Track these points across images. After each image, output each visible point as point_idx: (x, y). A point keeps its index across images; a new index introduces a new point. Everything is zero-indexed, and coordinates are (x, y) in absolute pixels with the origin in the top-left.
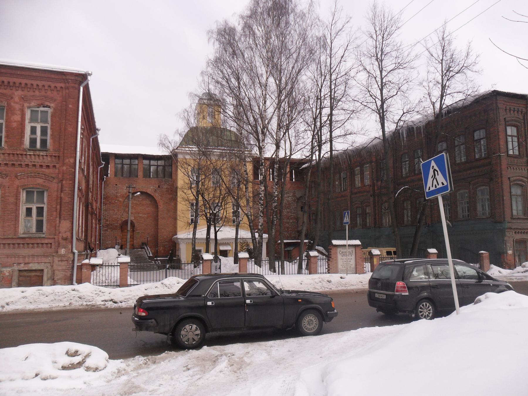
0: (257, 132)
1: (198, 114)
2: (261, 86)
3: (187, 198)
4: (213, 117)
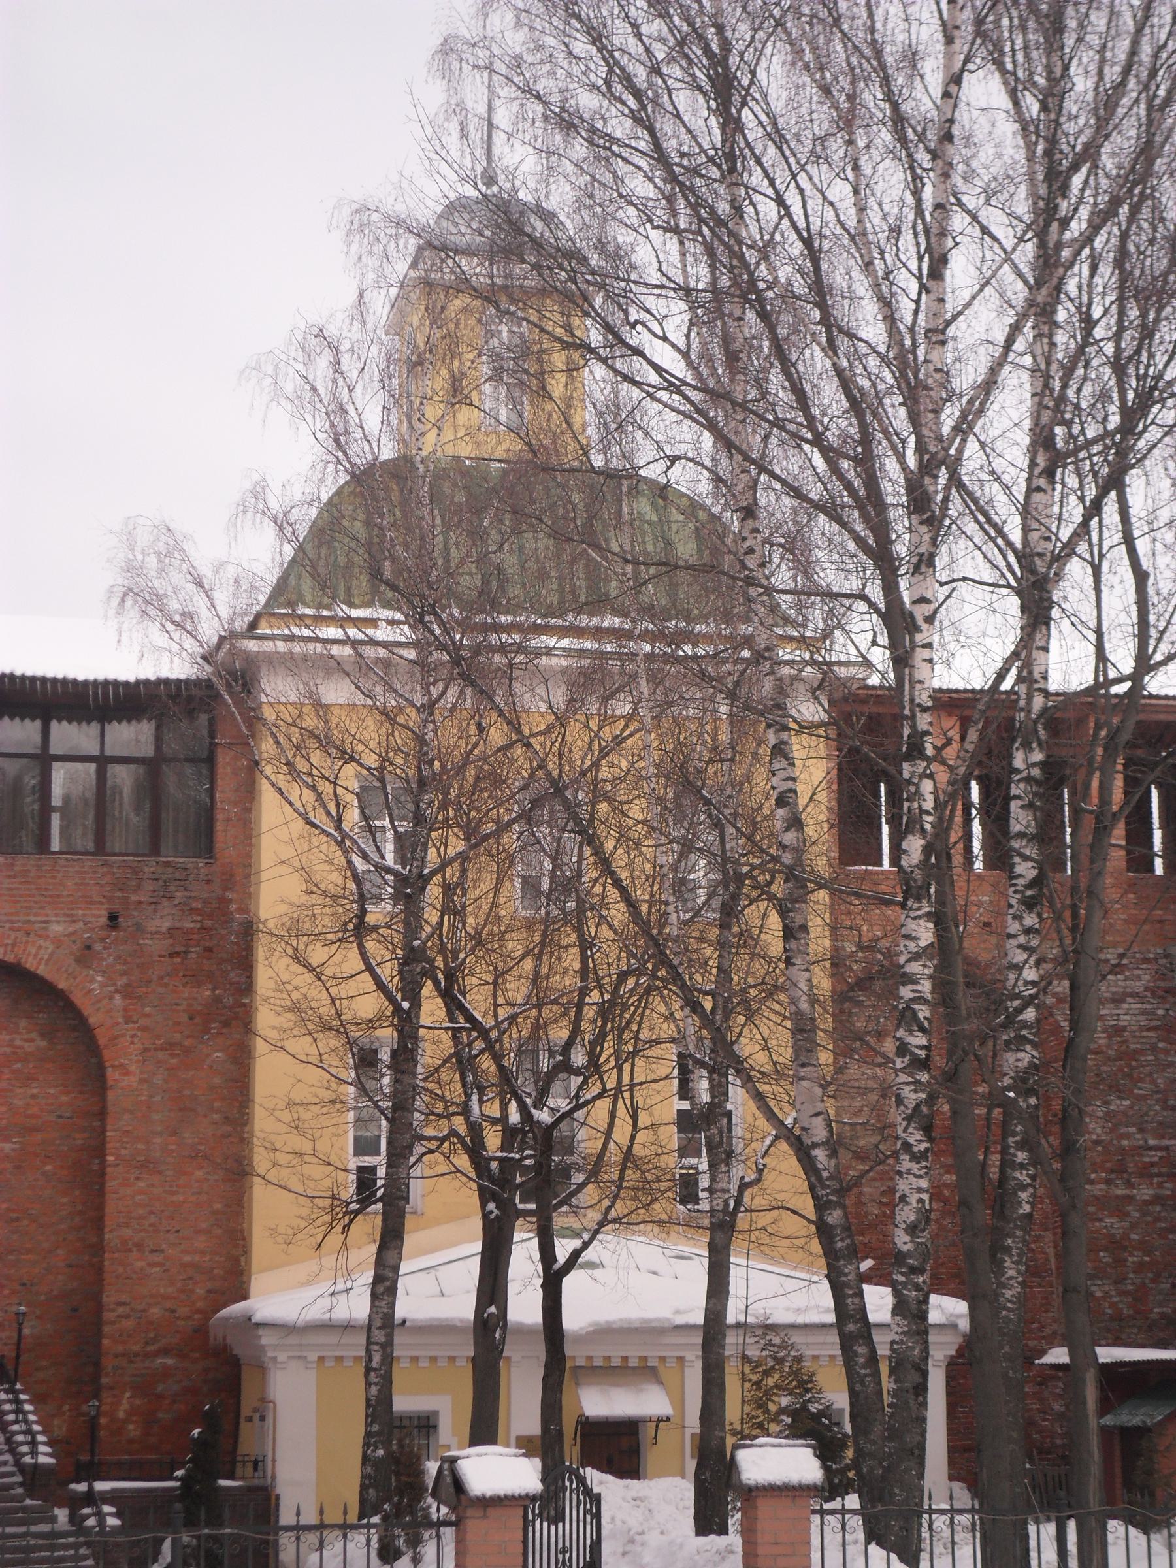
0: (872, 502)
1: (416, 365)
2: (902, 140)
3: (326, 1010)
4: (525, 373)
